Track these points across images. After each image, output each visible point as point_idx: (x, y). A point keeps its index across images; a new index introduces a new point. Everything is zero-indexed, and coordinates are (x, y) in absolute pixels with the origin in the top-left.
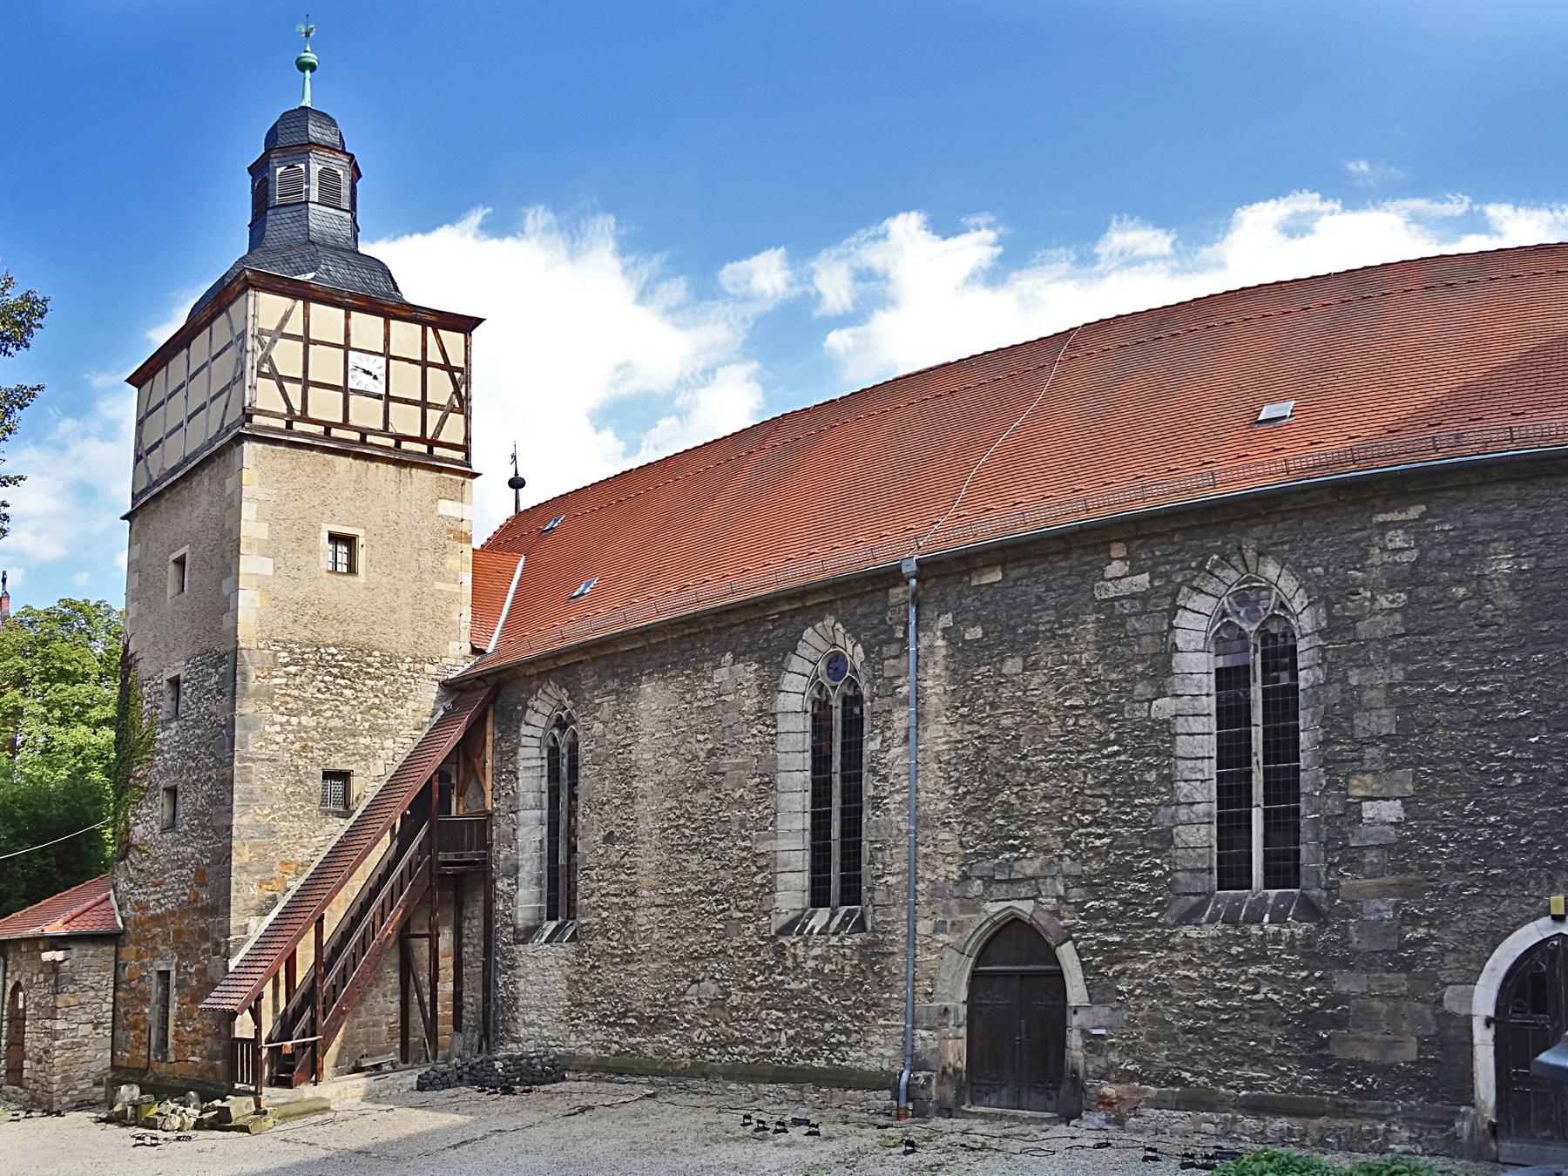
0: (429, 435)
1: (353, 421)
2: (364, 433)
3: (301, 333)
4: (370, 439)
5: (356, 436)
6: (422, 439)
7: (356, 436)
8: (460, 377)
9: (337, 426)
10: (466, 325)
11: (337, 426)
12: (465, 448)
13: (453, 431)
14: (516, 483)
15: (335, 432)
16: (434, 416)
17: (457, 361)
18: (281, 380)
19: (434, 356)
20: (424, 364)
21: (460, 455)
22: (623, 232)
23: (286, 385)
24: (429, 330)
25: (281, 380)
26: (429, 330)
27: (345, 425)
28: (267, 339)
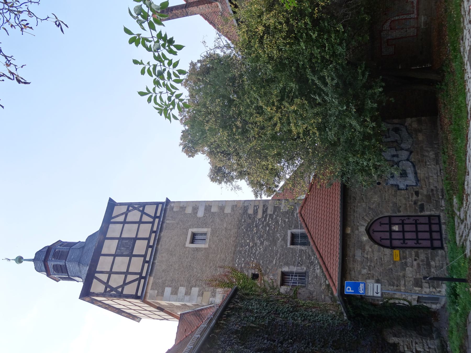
0: (151, 220)
1: (148, 236)
2: (152, 231)
3: (113, 270)
4: (155, 229)
5: (153, 235)
6: (153, 223)
7: (153, 235)
8: (131, 206)
9: (149, 242)
10: (112, 204)
11: (149, 242)
12: (157, 204)
13: (150, 210)
14: (20, 260)
15: (151, 244)
16: (145, 219)
17: (124, 209)
18: (125, 284)
19: (121, 219)
20: (125, 222)
21: (160, 206)
22: (228, 210)
23: (127, 281)
24: (112, 220)
25: (125, 284)
26: (112, 220)
27: (149, 239)
28: (108, 289)
